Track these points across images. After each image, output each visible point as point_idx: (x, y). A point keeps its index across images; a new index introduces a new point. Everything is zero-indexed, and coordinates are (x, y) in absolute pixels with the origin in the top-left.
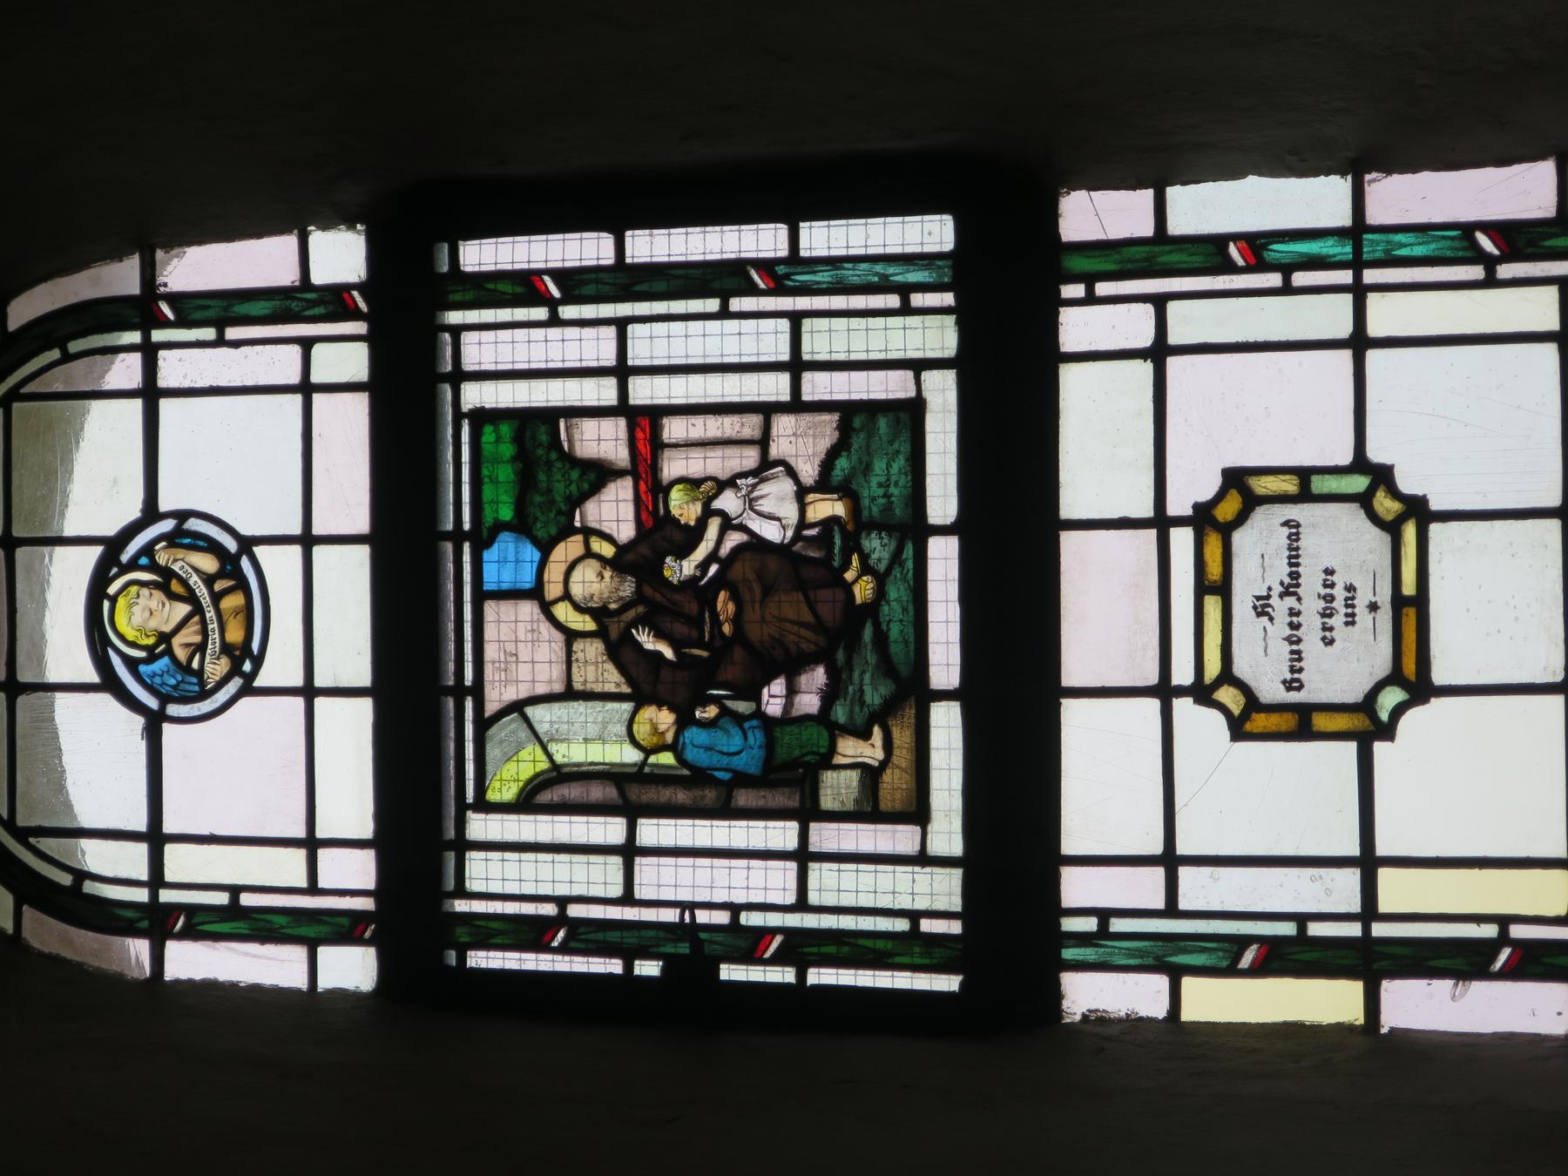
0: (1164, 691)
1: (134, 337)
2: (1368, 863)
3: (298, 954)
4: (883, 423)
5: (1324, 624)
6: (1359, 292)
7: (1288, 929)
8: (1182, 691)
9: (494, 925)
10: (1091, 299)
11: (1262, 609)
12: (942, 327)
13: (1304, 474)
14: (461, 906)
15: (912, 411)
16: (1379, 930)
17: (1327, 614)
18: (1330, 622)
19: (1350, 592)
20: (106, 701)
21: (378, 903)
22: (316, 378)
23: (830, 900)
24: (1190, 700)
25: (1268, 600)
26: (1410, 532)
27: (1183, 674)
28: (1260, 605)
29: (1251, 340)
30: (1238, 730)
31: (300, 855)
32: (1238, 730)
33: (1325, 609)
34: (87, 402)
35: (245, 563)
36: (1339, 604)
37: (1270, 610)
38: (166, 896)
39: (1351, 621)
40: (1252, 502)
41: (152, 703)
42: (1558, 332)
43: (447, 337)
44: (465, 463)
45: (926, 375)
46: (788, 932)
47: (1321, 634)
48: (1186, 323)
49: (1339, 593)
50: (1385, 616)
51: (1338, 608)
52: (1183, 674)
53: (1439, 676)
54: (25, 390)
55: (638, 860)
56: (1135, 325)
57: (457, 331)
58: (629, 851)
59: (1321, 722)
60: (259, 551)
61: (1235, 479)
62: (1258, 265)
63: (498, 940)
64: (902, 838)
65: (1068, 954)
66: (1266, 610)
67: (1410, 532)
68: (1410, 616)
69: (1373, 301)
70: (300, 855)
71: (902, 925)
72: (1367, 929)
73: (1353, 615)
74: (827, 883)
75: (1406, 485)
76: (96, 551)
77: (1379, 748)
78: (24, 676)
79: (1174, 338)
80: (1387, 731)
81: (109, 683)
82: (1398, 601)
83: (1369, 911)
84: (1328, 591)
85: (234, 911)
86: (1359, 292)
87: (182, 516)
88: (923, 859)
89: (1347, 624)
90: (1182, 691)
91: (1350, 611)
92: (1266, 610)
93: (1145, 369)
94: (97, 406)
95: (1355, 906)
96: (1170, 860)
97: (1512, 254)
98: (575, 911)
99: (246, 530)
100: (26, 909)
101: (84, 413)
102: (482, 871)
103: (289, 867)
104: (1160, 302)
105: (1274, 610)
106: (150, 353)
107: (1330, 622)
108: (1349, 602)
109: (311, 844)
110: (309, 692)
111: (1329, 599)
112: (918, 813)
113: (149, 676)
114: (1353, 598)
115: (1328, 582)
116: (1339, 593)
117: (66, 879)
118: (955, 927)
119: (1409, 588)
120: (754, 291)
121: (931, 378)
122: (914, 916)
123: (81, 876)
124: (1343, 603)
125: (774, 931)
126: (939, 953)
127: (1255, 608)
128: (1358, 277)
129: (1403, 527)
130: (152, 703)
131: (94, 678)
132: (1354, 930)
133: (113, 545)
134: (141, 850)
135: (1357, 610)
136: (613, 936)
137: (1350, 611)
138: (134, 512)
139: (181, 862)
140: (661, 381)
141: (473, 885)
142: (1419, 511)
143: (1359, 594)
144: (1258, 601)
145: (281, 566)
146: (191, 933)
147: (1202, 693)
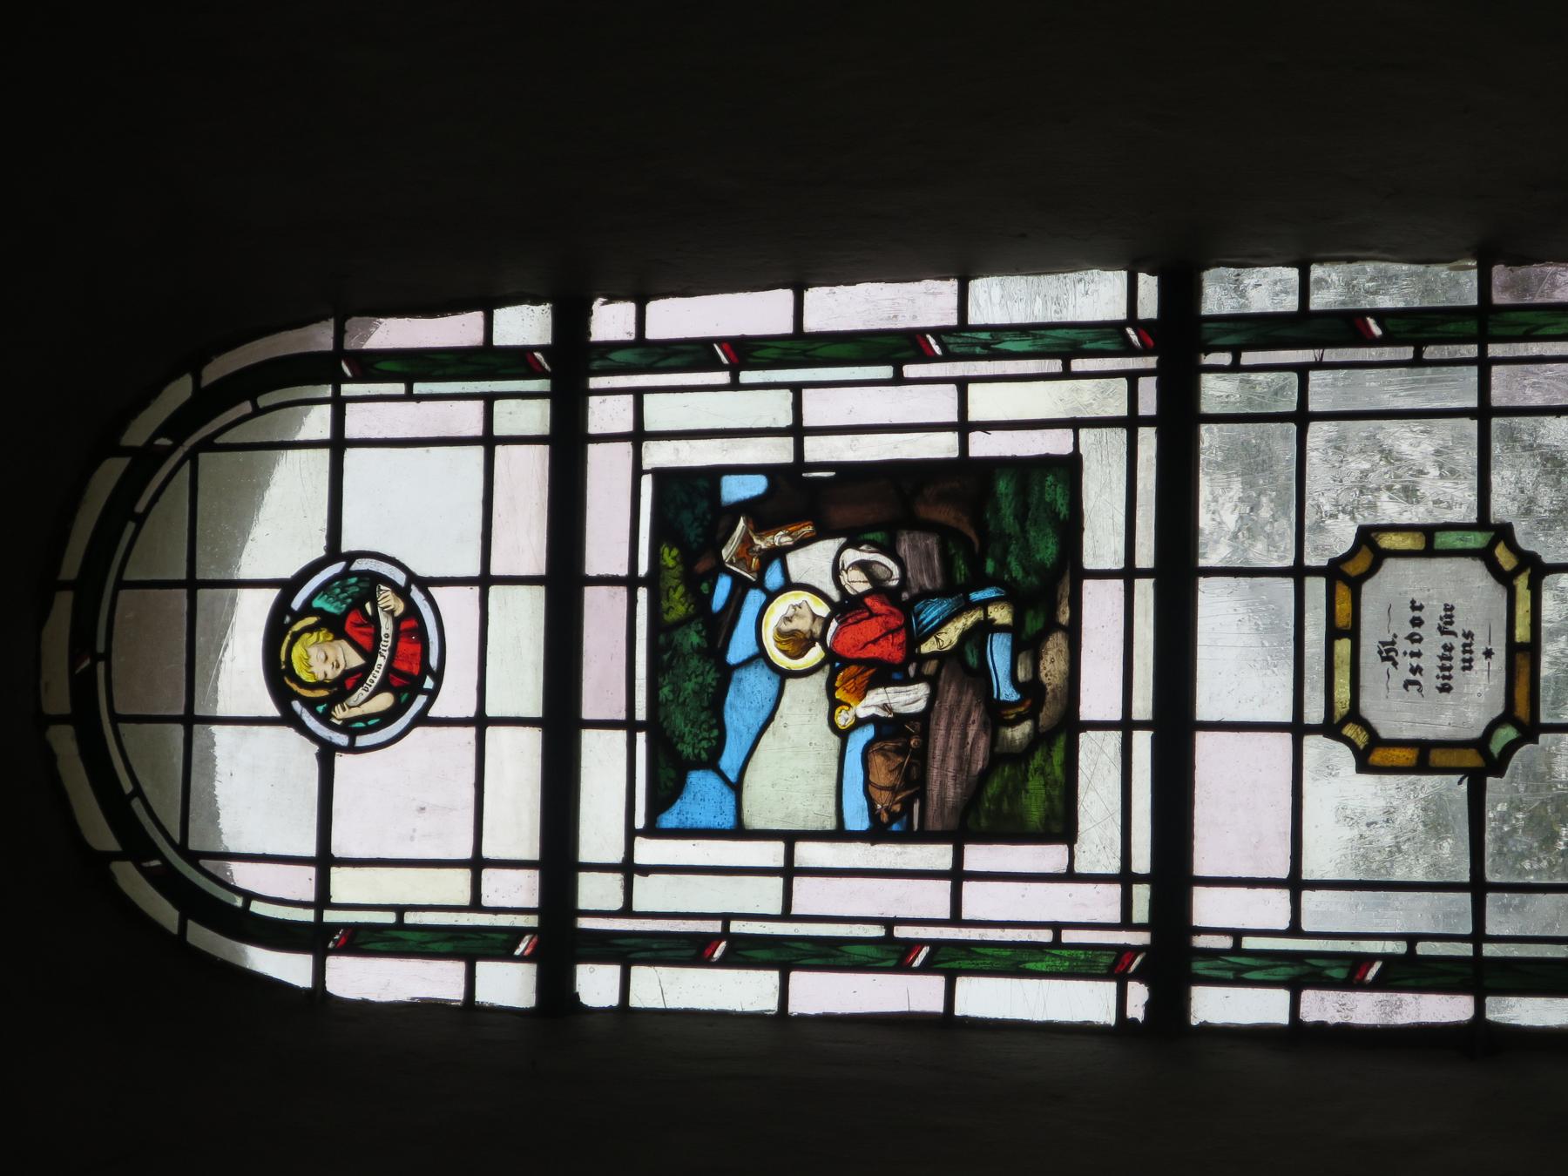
0: (1298, 729)
2: (1478, 887)
3: (457, 969)
6: (1484, 365)
8: (1314, 730)
11: (1388, 653)
15: (1070, 468)
16: (1489, 950)
19: (1467, 639)
22: (499, 430)
26: (1522, 583)
29: (672, 395)
30: (1364, 766)
31: (465, 875)
32: (1364, 766)
34: (273, 452)
35: (643, 568)
37: (1393, 654)
38: (330, 916)
39: (1468, 665)
42: (964, 880)
46: (936, 944)
49: (1458, 642)
52: (1314, 713)
54: (220, 440)
56: (1278, 392)
59: (1437, 757)
64: (1050, 857)
65: (1199, 967)
67: (1522, 583)
74: (980, 901)
76: (272, 594)
78: (199, 711)
80: (1498, 766)
81: (289, 719)
82: (1513, 648)
86: (1484, 365)
87: (352, 557)
88: (1070, 876)
89: (1464, 669)
91: (1467, 656)
98: (736, 927)
99: (422, 570)
101: (275, 463)
106: (339, 405)
109: (477, 864)
110: (481, 722)
114: (1470, 645)
120: (931, 358)
121: (647, 463)
125: (921, 943)
127: (1380, 652)
128: (1483, 350)
131: (272, 711)
132: (1466, 950)
133: (288, 587)
135: (1461, 656)
137: (1467, 656)
138: (320, 552)
139: (346, 885)
144: (1384, 646)
145: (457, 606)
147: (1331, 728)
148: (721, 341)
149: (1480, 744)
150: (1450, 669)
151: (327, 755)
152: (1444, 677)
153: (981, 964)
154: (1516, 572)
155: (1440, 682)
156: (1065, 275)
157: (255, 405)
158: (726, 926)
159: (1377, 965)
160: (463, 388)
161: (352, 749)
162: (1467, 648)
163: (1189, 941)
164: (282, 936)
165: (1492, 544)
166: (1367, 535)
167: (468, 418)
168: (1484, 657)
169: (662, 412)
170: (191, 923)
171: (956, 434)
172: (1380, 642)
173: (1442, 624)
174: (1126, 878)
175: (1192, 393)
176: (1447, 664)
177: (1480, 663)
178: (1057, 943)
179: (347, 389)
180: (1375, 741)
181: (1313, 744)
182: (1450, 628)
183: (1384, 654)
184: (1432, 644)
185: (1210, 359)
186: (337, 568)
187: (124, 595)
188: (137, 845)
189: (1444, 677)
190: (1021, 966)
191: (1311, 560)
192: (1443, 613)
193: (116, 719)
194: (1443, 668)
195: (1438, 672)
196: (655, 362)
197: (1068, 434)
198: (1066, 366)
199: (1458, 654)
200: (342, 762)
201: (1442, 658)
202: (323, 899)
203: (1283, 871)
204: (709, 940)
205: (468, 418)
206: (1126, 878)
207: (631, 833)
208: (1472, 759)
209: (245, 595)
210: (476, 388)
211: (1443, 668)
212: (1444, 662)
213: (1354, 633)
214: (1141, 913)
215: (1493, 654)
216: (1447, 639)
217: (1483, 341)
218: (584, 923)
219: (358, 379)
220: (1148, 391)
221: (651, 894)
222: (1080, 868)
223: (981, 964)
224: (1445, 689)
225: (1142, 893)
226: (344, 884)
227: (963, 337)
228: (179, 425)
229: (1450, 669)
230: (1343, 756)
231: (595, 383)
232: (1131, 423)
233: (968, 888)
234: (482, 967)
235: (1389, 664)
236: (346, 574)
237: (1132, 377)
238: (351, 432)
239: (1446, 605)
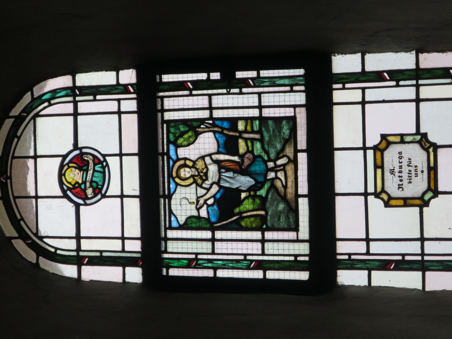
0: (366, 194)
4: (284, 122)
6: (418, 86)
7: (400, 258)
8: (371, 194)
9: (71, 258)
11: (392, 172)
12: (264, 96)
13: (402, 136)
14: (166, 256)
15: (293, 120)
20: (65, 200)
21: (142, 255)
22: (422, 96)
23: (271, 252)
24: (373, 196)
26: (431, 150)
27: (371, 189)
30: (387, 205)
32: (387, 205)
37: (394, 173)
39: (416, 175)
40: (389, 143)
43: (159, 100)
44: (165, 133)
46: (256, 261)
48: (370, 95)
49: (412, 169)
52: (371, 189)
53: (440, 189)
55: (216, 242)
56: (356, 96)
57: (162, 98)
58: (213, 240)
61: (384, 137)
63: (70, 262)
64: (291, 235)
66: (393, 173)
67: (431, 150)
68: (432, 173)
69: (421, 88)
73: (417, 174)
76: (60, 159)
77: (425, 209)
79: (367, 99)
80: (427, 204)
81: (65, 196)
85: (403, 261)
86: (418, 86)
87: (81, 149)
88: (298, 241)
89: (415, 176)
90: (371, 194)
91: (416, 173)
92: (393, 173)
93: (123, 116)
96: (422, 239)
97: (196, 88)
99: (103, 152)
100: (40, 258)
102: (172, 246)
103: (116, 245)
104: (363, 89)
105: (395, 173)
110: (122, 196)
112: (296, 229)
114: (417, 169)
118: (307, 259)
119: (432, 164)
120: (250, 86)
122: (296, 256)
126: (415, 266)
129: (248, 153)
131: (61, 194)
133: (64, 157)
134: (74, 241)
135: (418, 173)
136: (407, 266)
140: (272, 110)
141: (169, 250)
142: (436, 147)
144: (391, 171)
145: (113, 162)
146: (89, 264)
147: (377, 195)
149: (422, 198)
150: (411, 177)
151: (77, 206)
152: (410, 179)
154: (429, 147)
155: (408, 181)
159: (85, 262)
160: (404, 83)
161: (86, 204)
162: (416, 170)
163: (336, 257)
164: (66, 260)
165: (421, 139)
166: (384, 137)
167: (113, 106)
170: (40, 258)
171: (209, 111)
172: (390, 169)
173: (408, 164)
176: (410, 175)
178: (245, 259)
179: (78, 98)
180: (390, 198)
181: (371, 198)
182: (410, 165)
183: (391, 173)
184: (405, 169)
186: (77, 152)
187: (14, 160)
188: (23, 236)
189: (410, 179)
191: (368, 145)
192: (408, 161)
193: (15, 198)
194: (409, 177)
195: (408, 178)
196: (260, 84)
197: (292, 109)
199: (413, 172)
200: (82, 208)
201: (409, 174)
202: (79, 249)
205: (113, 106)
211: (409, 177)
212: (409, 175)
213: (382, 167)
215: (421, 172)
216: (410, 168)
219: (81, 95)
224: (410, 182)
228: (28, 109)
229: (411, 177)
235: (393, 175)
238: (80, 110)
239: (409, 158)
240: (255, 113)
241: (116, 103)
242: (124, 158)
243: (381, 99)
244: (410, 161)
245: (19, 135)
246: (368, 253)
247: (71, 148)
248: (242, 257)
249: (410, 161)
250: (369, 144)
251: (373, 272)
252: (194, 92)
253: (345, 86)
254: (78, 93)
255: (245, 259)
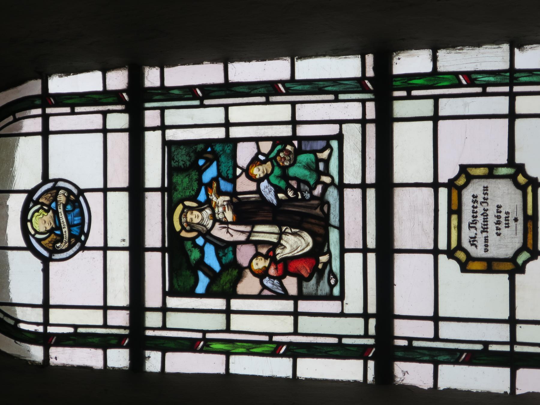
0: (435, 252)
1: (39, 111)
5: (497, 227)
8: (443, 252)
10: (409, 97)
17: (498, 223)
18: (499, 226)
20: (28, 254)
25: (475, 238)
26: (530, 189)
27: (443, 245)
28: (472, 241)
31: (100, 312)
32: (464, 269)
33: (497, 221)
35: (81, 199)
36: (503, 220)
37: (475, 243)
38: (50, 330)
40: (470, 178)
41: (45, 254)
45: (344, 126)
46: (290, 344)
47: (496, 231)
49: (503, 215)
50: (520, 226)
51: (502, 221)
52: (443, 245)
59: (495, 266)
60: (86, 194)
61: (464, 169)
62: (471, 83)
64: (333, 306)
68: (530, 225)
69: (519, 99)
70: (100, 312)
71: (335, 341)
72: (512, 348)
73: (508, 224)
75: (532, 171)
76: (24, 196)
77: (519, 277)
79: (441, 113)
80: (521, 270)
81: (30, 247)
83: (513, 341)
84: (499, 214)
87: (56, 181)
88: (342, 315)
89: (506, 227)
90: (443, 252)
91: (507, 222)
93: (109, 135)
94: (22, 139)
95: (508, 339)
96: (436, 319)
99: (82, 187)
103: (96, 318)
106: (45, 118)
107: (499, 226)
108: (507, 219)
109: (105, 308)
110: (105, 248)
111: (499, 217)
113: (46, 245)
114: (508, 217)
115: (498, 211)
116: (503, 215)
117: (12, 322)
119: (530, 212)
120: (281, 94)
123: (18, 321)
124: (504, 219)
127: (470, 242)
128: (511, 89)
130: (45, 254)
131: (23, 244)
132: (507, 348)
133: (31, 193)
135: (509, 222)
137: (507, 222)
143: (510, 216)
147: (450, 253)
148: (463, 73)
149: (513, 259)
153: (482, 362)
156: (368, 55)
157: (14, 117)
158: (204, 335)
162: (507, 219)
166: (464, 169)
167: (96, 121)
168: (514, 221)
169: (172, 117)
174: (365, 316)
175: (390, 109)
177: (512, 223)
178: (271, 341)
180: (470, 258)
185: (396, 94)
186: (49, 185)
190: (436, 358)
197: (337, 126)
198: (267, 99)
200: (53, 266)
203: (431, 313)
204: (195, 341)
206: (365, 316)
207: (165, 294)
208: (509, 266)
209: (12, 196)
210: (305, 98)
214: (372, 331)
217: (511, 85)
218: (149, 333)
220: (371, 107)
221: (173, 320)
222: (346, 311)
223: (482, 362)
225: (372, 322)
226: (55, 316)
227: (502, 75)
230: (454, 265)
231: (147, 105)
232: (363, 122)
233: (301, 319)
234: (300, 361)
236: (54, 188)
237: (363, 102)
238: (52, 128)
240: (286, 131)
241: (100, 117)
242: (109, 194)
243: (41, 274)
244: (486, 223)
245: (395, 95)
246: (436, 338)
247: (40, 181)
248: (266, 338)
249: (486, 223)
250: (443, 178)
251: (441, 367)
252: (206, 102)
253: (412, 93)
254: (199, 92)
255: (271, 341)
